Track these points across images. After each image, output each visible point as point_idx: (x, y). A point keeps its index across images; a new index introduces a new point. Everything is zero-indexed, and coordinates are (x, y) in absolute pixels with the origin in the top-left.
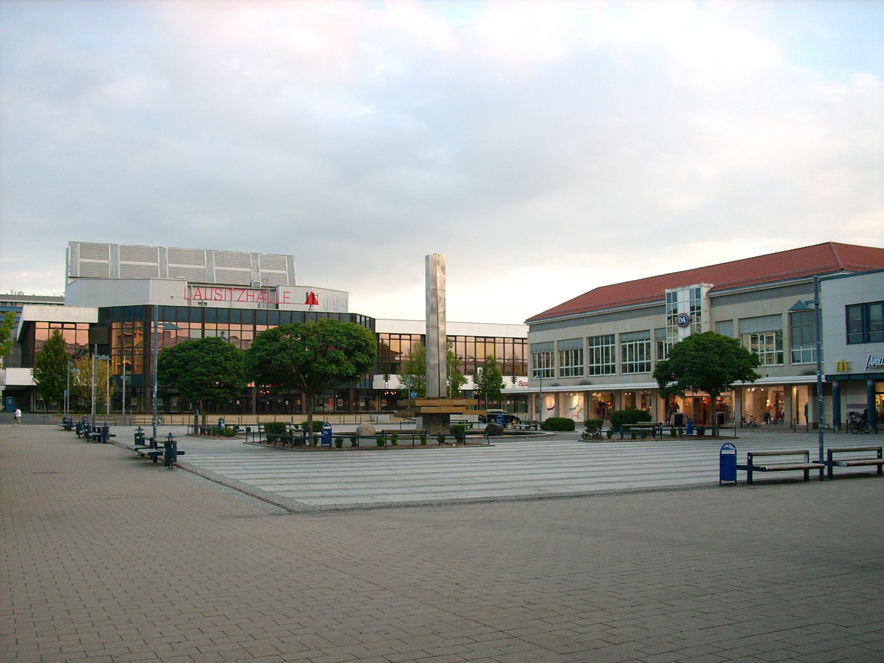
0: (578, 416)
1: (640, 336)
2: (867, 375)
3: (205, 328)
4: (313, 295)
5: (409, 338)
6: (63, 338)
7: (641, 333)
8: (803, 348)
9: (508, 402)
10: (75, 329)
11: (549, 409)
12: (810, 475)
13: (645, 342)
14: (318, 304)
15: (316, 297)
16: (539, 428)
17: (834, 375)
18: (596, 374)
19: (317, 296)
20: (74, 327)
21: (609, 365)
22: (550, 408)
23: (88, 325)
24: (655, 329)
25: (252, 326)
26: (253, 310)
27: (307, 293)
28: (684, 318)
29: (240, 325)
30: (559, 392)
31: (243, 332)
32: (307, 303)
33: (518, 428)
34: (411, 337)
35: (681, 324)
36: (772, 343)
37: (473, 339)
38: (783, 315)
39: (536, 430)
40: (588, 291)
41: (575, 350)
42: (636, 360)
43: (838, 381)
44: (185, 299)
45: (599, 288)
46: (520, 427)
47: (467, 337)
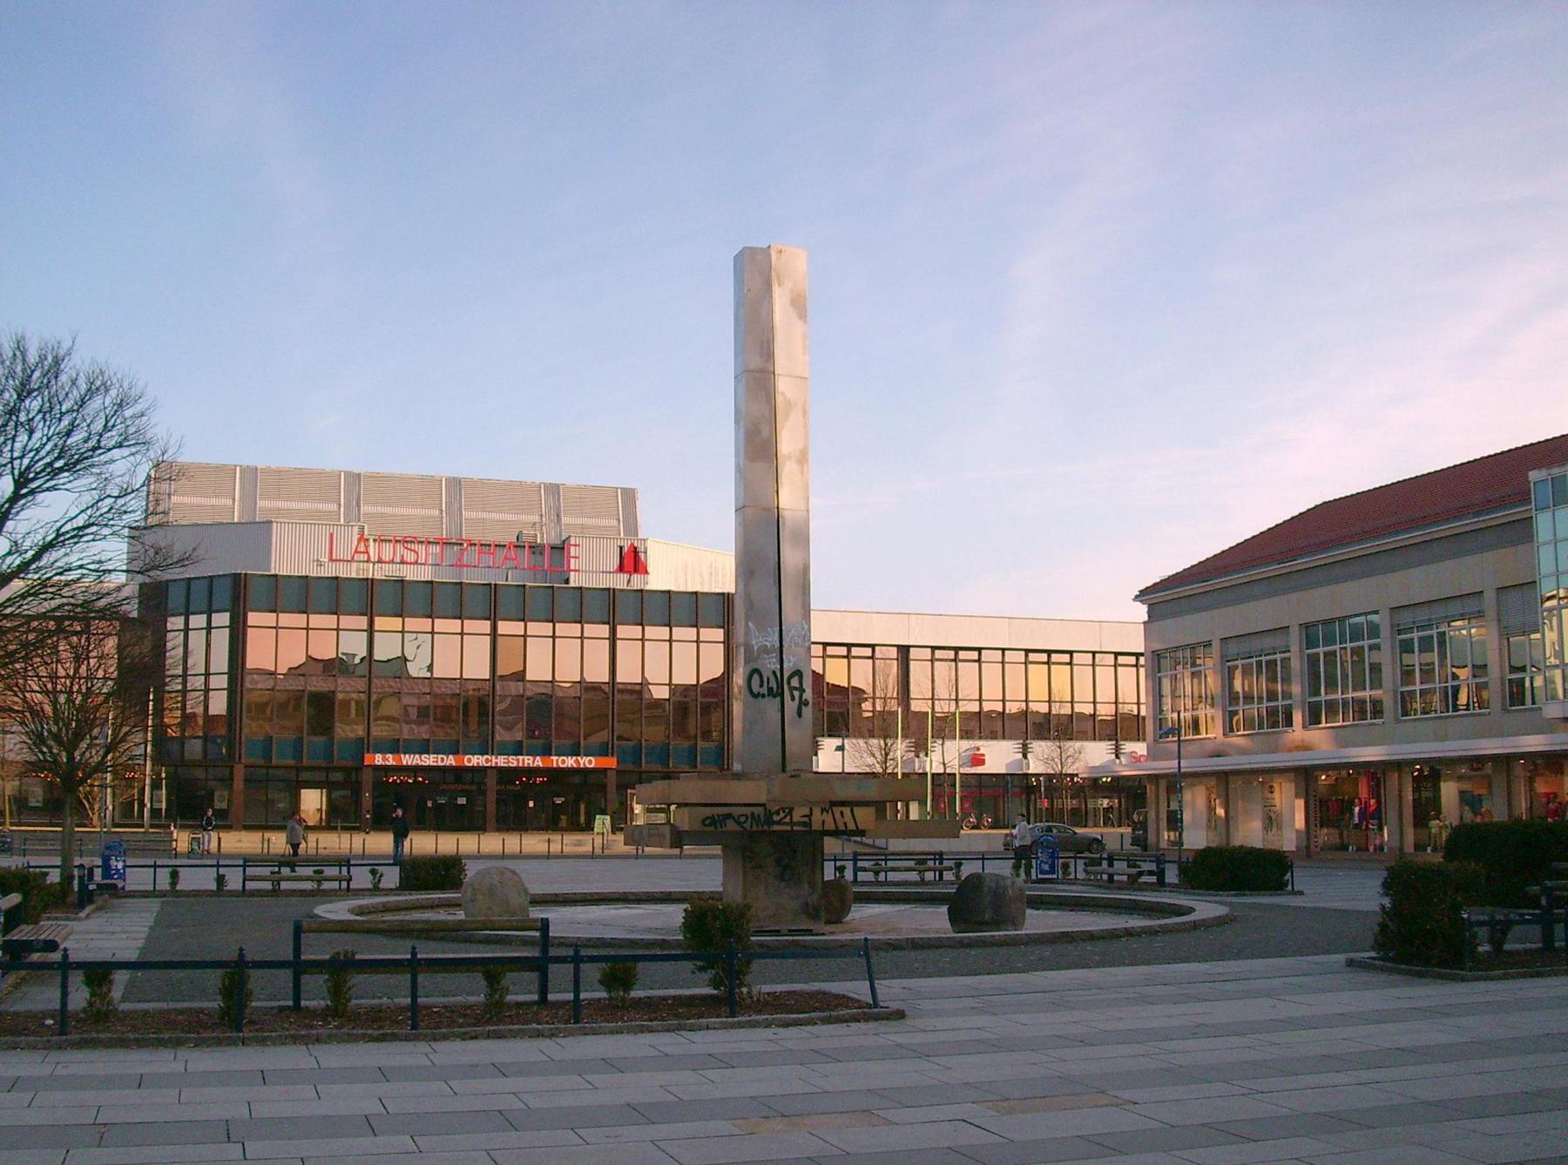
1: (1268, 642)
3: (499, 632)
5: (870, 654)
9: (1105, 803)
10: (872, 657)
13: (1278, 657)
16: (1172, 875)
19: (645, 552)
20: (845, 654)
21: (1278, 706)
23: (895, 649)
26: (723, 594)
27: (621, 548)
31: (585, 640)
32: (621, 569)
33: (1105, 877)
34: (873, 651)
36: (1433, 651)
39: (1161, 883)
40: (1210, 555)
46: (1111, 876)
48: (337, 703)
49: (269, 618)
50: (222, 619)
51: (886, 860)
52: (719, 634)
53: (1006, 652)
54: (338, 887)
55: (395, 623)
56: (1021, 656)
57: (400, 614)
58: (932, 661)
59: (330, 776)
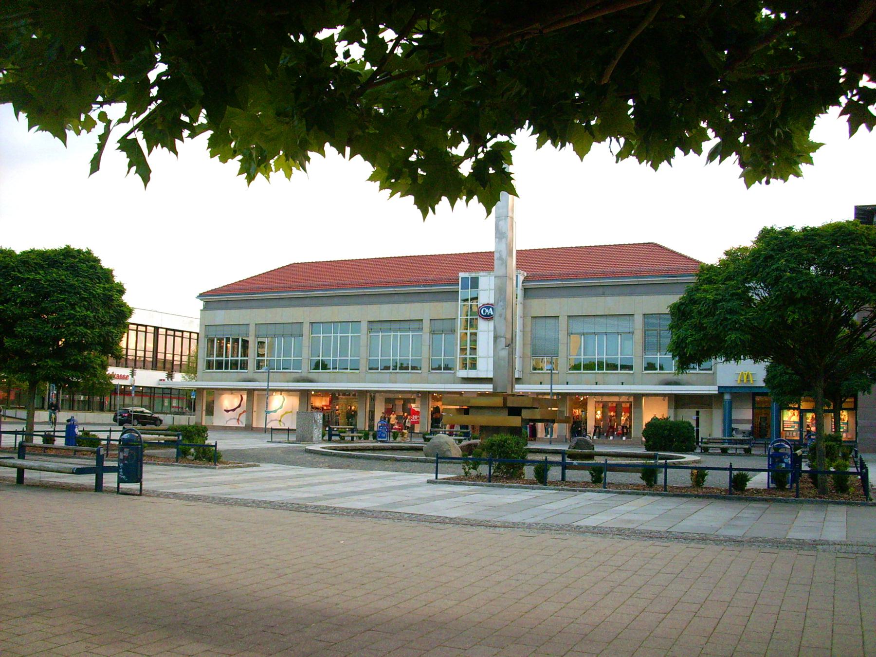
0: (280, 421)
2: (153, 389)
6: (304, 122)
7: (408, 323)
8: (660, 355)
9: (82, 398)
11: (227, 411)
12: (25, 476)
17: (155, 388)
18: (322, 369)
22: (229, 409)
24: (431, 320)
28: (491, 309)
30: (254, 390)
35: (487, 315)
38: (635, 316)
41: (227, 338)
42: (279, 356)
43: (731, 394)
45: (295, 263)
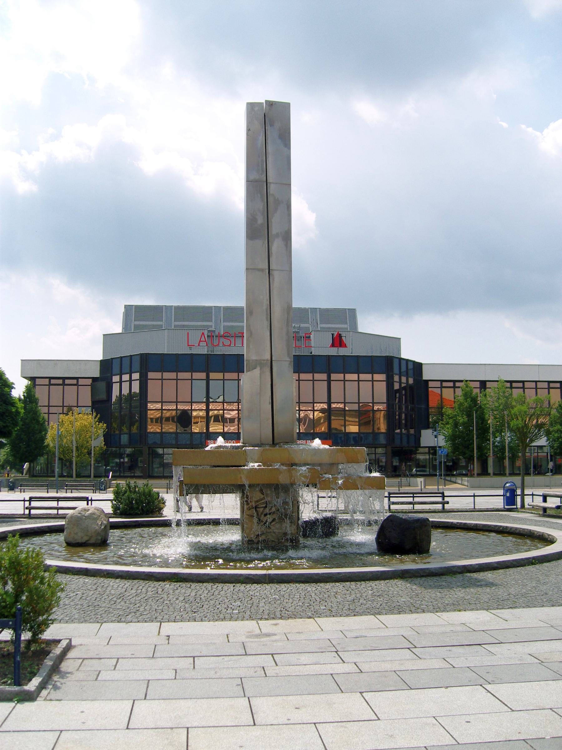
4: (340, 336)
10: (77, 385)
14: (345, 346)
15: (343, 338)
25: (326, 374)
27: (333, 334)
29: (357, 375)
32: (333, 345)
37: (546, 385)
44: (305, 334)
47: (538, 383)
48: (193, 418)
49: (158, 375)
50: (136, 376)
51: (413, 497)
52: (383, 377)
53: (538, 383)
54: (56, 513)
55: (220, 375)
56: (533, 385)
57: (358, 372)
58: (536, 388)
59: (376, 451)
